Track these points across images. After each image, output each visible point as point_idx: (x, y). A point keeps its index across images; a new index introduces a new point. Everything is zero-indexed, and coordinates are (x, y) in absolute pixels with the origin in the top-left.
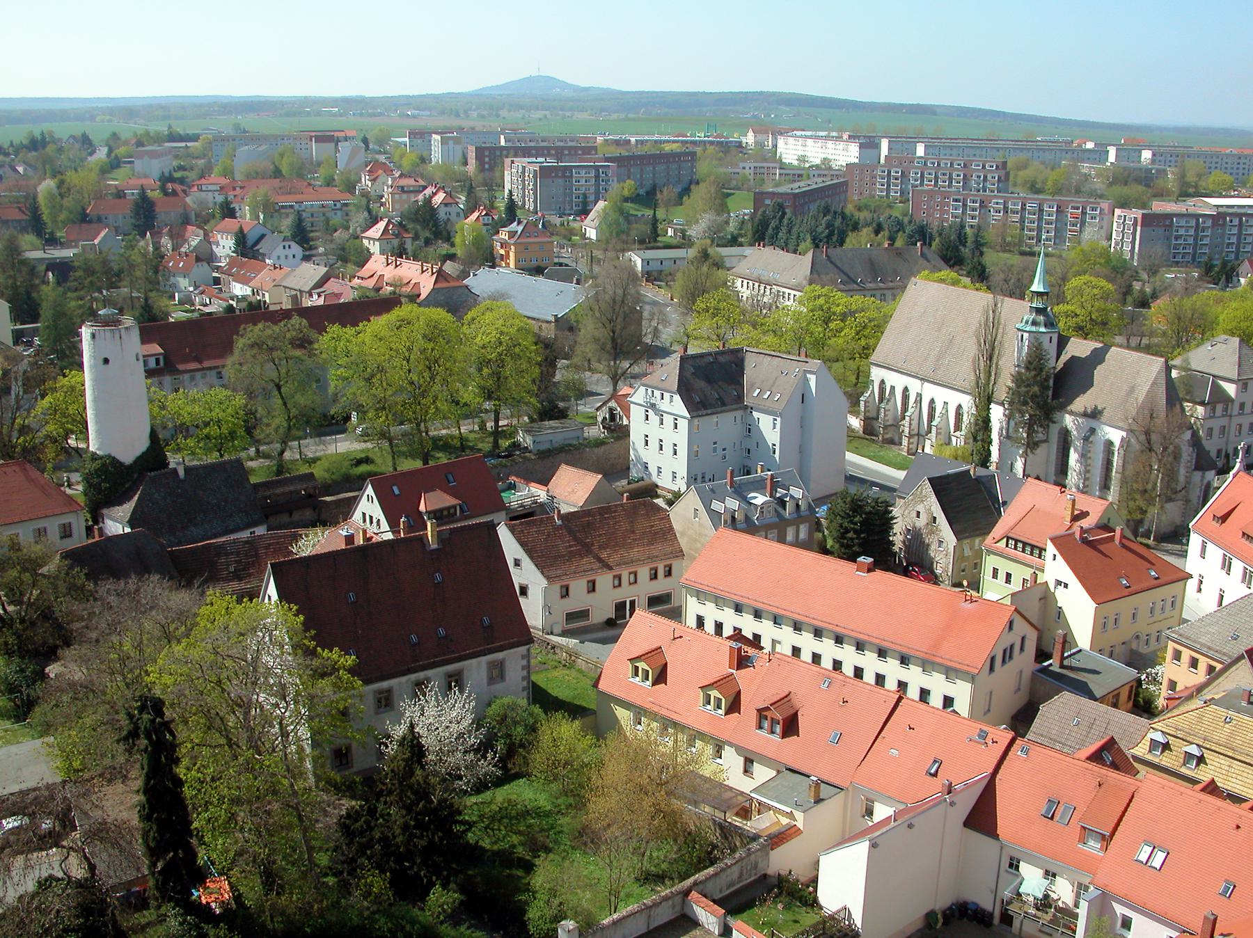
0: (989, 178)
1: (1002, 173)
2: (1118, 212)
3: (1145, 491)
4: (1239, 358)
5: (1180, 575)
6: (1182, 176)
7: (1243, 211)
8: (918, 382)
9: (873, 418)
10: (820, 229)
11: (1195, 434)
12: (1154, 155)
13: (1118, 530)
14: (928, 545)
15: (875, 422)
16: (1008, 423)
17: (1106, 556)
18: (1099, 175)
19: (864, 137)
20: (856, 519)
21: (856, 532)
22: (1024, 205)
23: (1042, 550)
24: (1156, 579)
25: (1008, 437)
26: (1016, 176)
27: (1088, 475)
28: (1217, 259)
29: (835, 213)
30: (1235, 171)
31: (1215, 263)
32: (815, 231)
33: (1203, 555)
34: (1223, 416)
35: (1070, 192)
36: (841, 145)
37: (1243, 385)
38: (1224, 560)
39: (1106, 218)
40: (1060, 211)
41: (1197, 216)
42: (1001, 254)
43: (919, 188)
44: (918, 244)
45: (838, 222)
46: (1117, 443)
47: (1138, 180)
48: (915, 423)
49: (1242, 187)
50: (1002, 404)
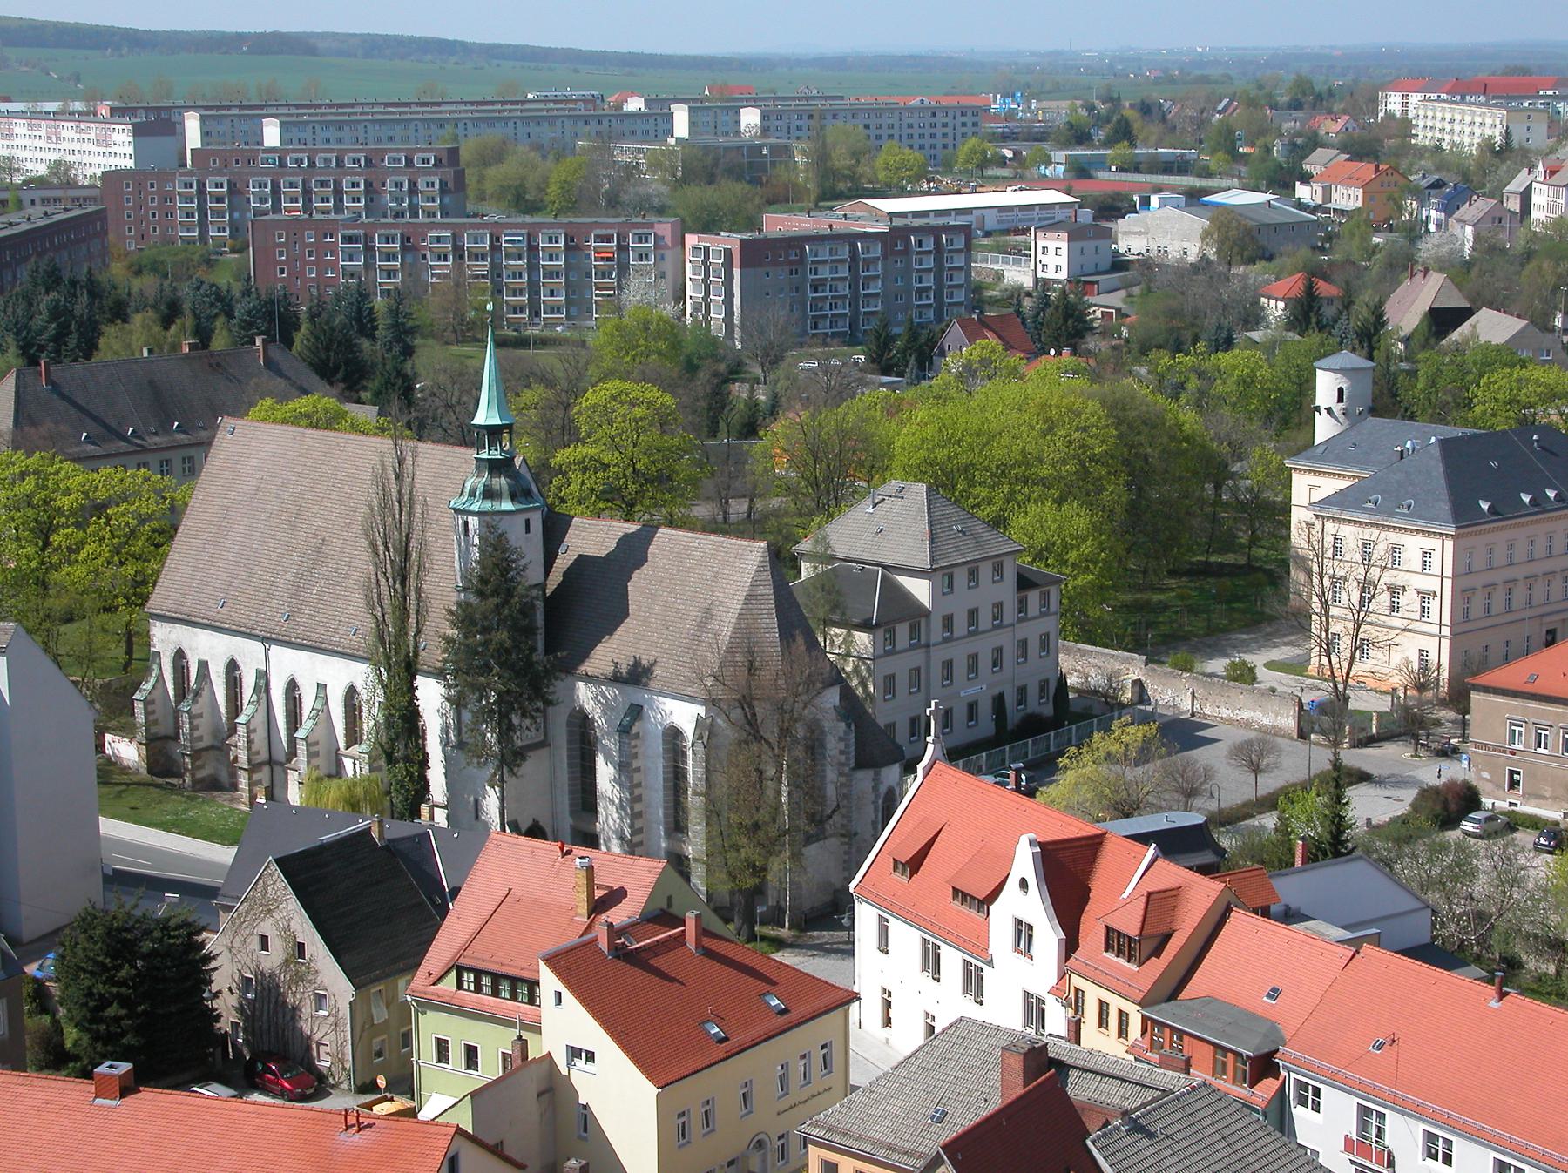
0: (421, 186)
1: (449, 173)
2: (691, 240)
3: (756, 826)
4: (931, 523)
5: (829, 999)
6: (821, 159)
7: (941, 221)
8: (258, 647)
9: (167, 738)
10: (38, 322)
11: (847, 693)
12: (764, 117)
13: (690, 918)
14: (295, 1009)
15: (171, 744)
16: (458, 717)
17: (672, 980)
18: (655, 165)
19: (147, 109)
20: (122, 974)
21: (124, 1002)
22: (495, 239)
23: (533, 985)
24: (783, 1012)
25: (461, 745)
26: (481, 179)
27: (638, 807)
28: (899, 324)
29: (73, 283)
30: (927, 142)
31: (896, 330)
32: (26, 327)
33: (883, 946)
34: (912, 647)
35: (596, 204)
36: (93, 130)
37: (940, 574)
38: (925, 951)
39: (669, 254)
40: (409, 245)
41: (851, 238)
42: (455, 349)
43: (271, 217)
44: (258, 341)
45: (81, 305)
46: (689, 730)
47: (735, 173)
48: (260, 737)
49: (944, 174)
50: (439, 674)
